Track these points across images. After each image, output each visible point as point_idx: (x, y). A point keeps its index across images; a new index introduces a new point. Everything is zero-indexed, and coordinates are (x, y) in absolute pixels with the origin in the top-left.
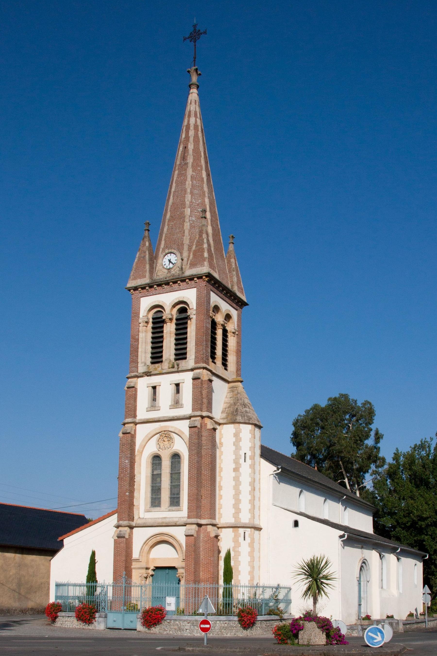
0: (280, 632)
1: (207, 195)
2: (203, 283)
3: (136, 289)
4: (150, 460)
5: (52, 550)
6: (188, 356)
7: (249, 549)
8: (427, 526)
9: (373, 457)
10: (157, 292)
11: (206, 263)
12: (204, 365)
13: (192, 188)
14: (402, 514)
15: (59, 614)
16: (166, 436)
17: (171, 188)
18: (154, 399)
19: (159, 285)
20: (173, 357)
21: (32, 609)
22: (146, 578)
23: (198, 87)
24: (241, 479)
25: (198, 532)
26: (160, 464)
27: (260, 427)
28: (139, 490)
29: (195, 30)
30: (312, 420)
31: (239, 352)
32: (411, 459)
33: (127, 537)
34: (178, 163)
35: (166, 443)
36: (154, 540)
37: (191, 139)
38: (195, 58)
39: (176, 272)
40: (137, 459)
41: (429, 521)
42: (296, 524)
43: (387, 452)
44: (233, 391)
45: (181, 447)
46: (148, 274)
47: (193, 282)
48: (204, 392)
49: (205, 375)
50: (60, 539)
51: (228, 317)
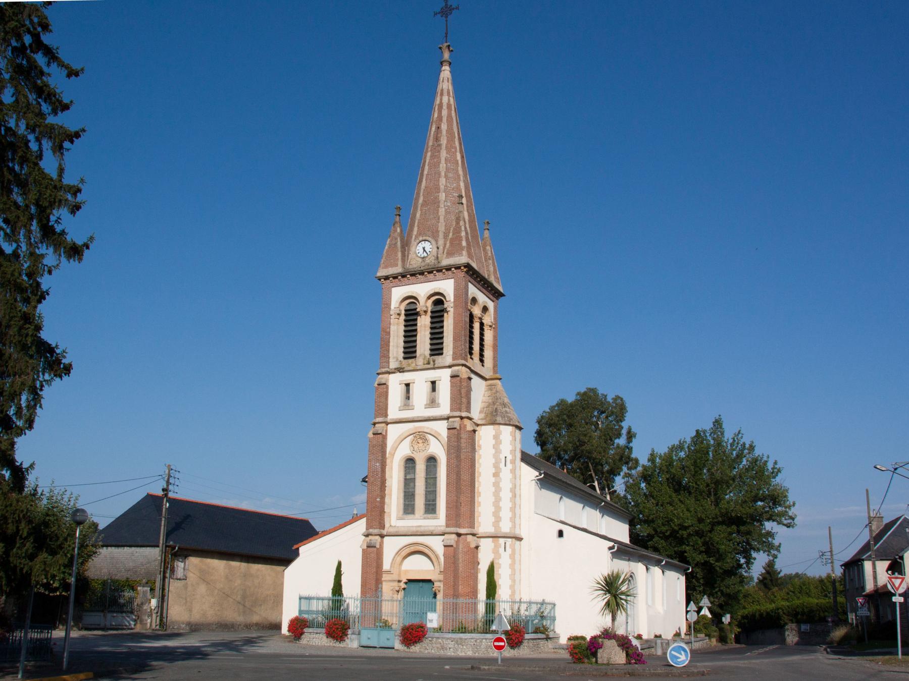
0: (577, 651)
1: (462, 178)
2: (461, 274)
3: (387, 278)
4: (403, 463)
5: (286, 559)
6: (445, 351)
7: (510, 561)
8: (689, 535)
9: (625, 458)
10: (410, 282)
11: (464, 253)
12: (463, 362)
13: (445, 171)
14: (660, 522)
15: (306, 630)
16: (421, 437)
17: (423, 171)
18: (408, 398)
19: (412, 275)
20: (428, 352)
21: (257, 624)
22: (398, 591)
23: (450, 64)
24: (501, 485)
25: (457, 542)
26: (414, 468)
27: (520, 428)
28: (391, 495)
29: (446, 4)
30: (558, 416)
31: (495, 347)
32: (668, 460)
33: (378, 546)
34: (431, 144)
35: (421, 445)
36: (408, 550)
37: (445, 119)
38: (446, 34)
39: (431, 261)
40: (388, 461)
41: (690, 530)
42: (561, 534)
43: (641, 453)
44: (491, 390)
45: (437, 449)
46: (400, 263)
47: (450, 272)
48: (463, 391)
49: (464, 372)
50: (295, 547)
51: (485, 309)
